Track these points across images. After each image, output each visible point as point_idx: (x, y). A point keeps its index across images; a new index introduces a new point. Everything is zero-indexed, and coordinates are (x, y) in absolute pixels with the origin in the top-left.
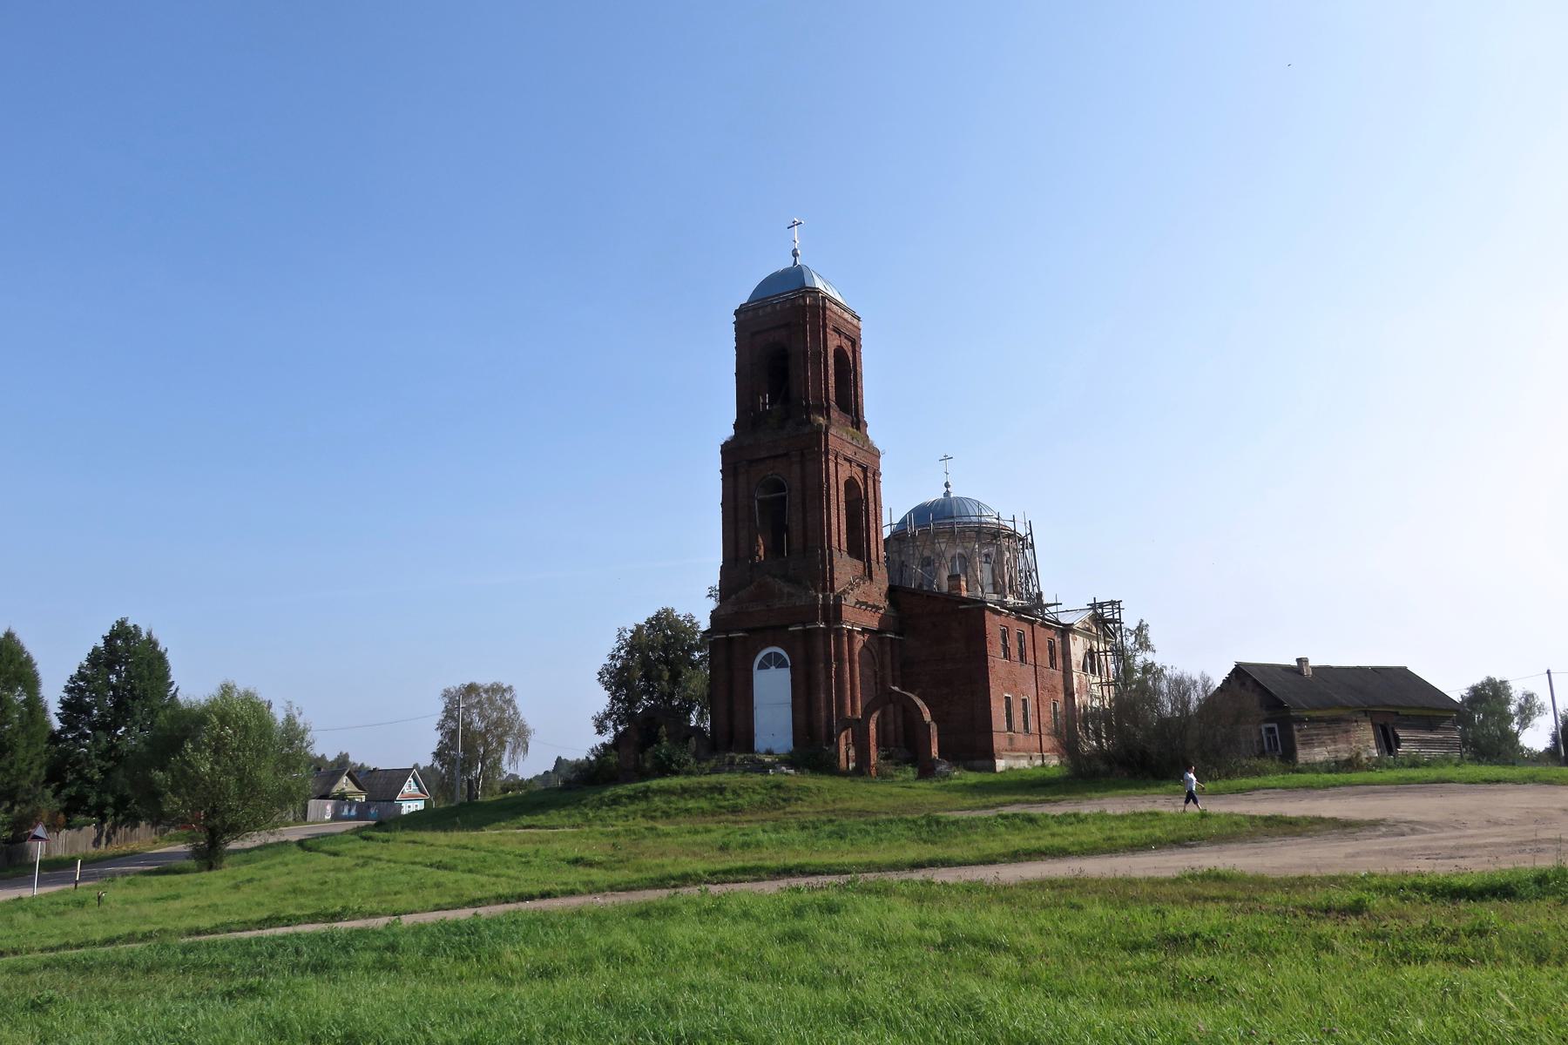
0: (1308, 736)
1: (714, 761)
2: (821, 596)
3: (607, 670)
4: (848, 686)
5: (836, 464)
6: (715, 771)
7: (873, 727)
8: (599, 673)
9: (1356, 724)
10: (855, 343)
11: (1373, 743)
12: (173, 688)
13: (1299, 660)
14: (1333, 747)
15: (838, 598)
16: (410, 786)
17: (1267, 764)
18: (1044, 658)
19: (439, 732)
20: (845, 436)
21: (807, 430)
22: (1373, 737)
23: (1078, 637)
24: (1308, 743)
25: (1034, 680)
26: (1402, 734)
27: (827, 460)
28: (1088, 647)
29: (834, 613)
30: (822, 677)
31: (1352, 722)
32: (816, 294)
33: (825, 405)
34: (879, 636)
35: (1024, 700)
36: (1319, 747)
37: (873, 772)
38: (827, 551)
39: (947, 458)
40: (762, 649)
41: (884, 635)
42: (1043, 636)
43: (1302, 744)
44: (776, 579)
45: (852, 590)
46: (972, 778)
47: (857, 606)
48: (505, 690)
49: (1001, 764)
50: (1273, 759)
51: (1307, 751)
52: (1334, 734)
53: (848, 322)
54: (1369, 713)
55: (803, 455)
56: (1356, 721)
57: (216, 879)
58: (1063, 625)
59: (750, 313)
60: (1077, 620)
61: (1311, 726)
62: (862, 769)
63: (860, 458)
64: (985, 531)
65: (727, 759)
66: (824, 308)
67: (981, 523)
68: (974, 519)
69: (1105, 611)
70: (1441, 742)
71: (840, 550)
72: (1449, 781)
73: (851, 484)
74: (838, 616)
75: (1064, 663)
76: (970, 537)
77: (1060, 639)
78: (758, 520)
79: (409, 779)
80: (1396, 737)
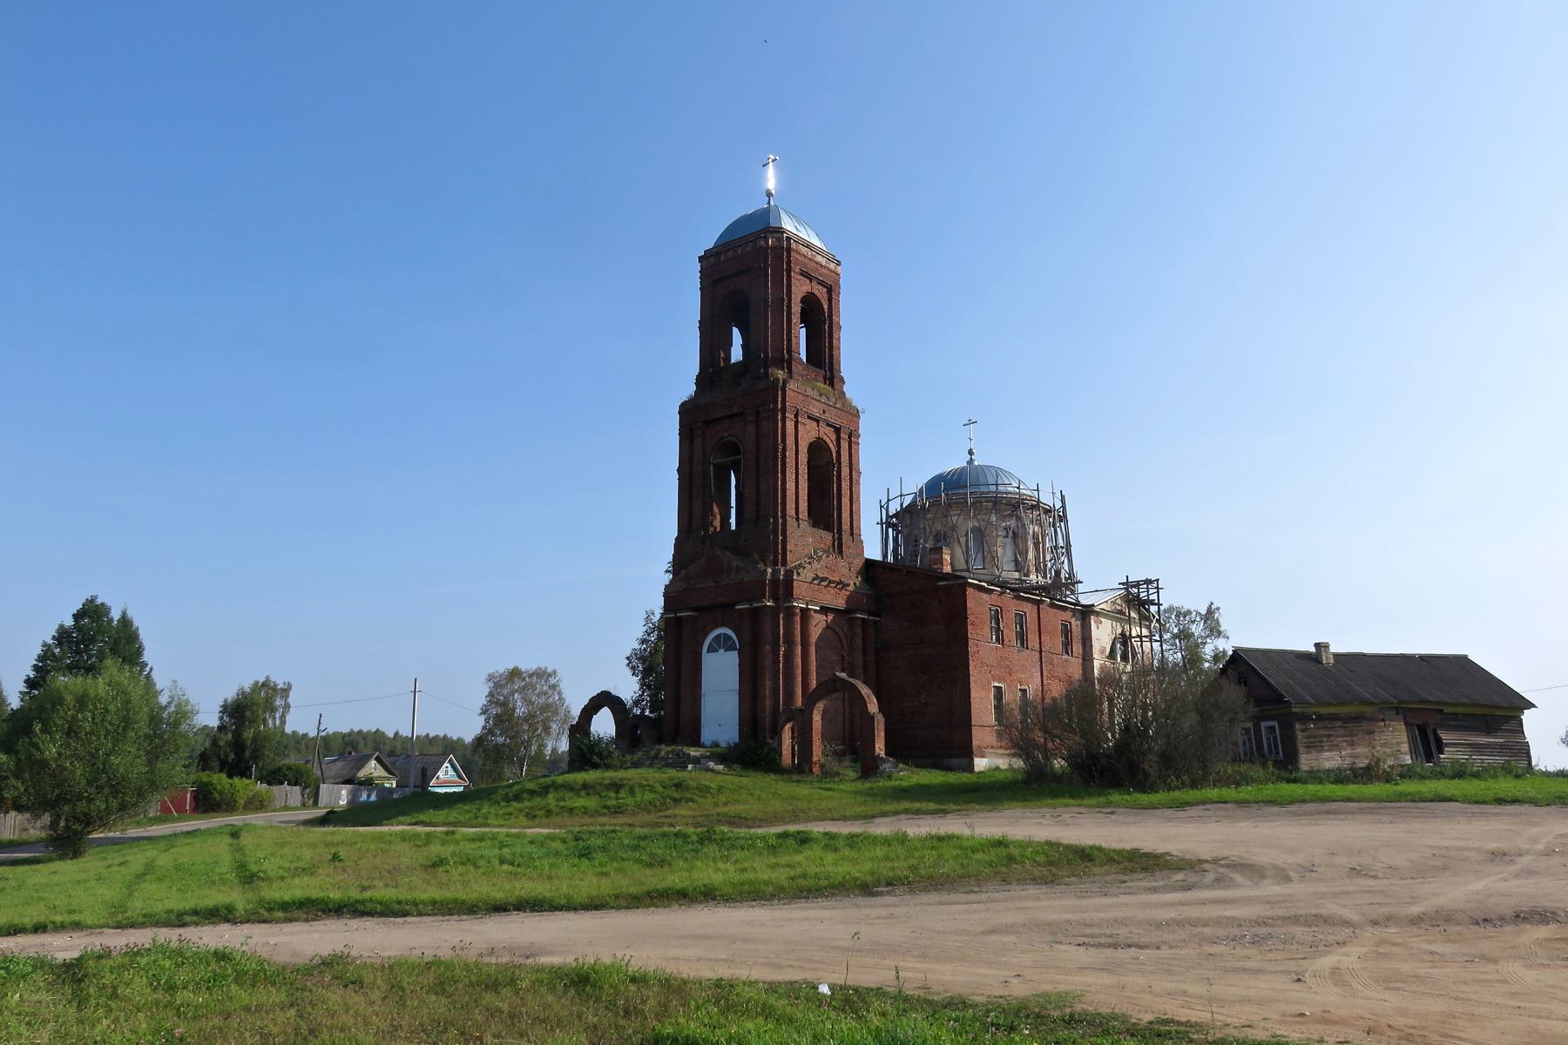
0: (1315, 737)
1: (641, 753)
2: (769, 570)
3: (636, 654)
4: (799, 672)
5: (796, 423)
6: (636, 765)
7: (817, 718)
8: (628, 658)
9: (1382, 724)
10: (831, 290)
11: (1405, 747)
12: (148, 669)
13: (1317, 645)
14: (1349, 751)
15: (789, 573)
16: (447, 773)
17: (1257, 771)
18: (1054, 642)
19: (483, 717)
20: (810, 392)
21: (763, 384)
22: (1406, 739)
23: (1103, 620)
24: (1315, 745)
25: (1039, 666)
26: (1446, 737)
27: (784, 419)
28: (1119, 631)
29: (784, 589)
30: (768, 663)
31: (1378, 721)
32: (780, 235)
33: (786, 355)
34: (849, 616)
35: (998, 689)
36: (1330, 750)
37: (816, 769)
38: (780, 521)
39: (971, 422)
40: (712, 629)
41: (854, 615)
42: (1053, 618)
43: (1307, 747)
44: (727, 552)
45: (810, 563)
46: (952, 778)
47: (816, 582)
48: (549, 675)
49: (980, 764)
50: (1264, 765)
51: (1314, 755)
52: (1351, 736)
53: (822, 266)
54: (1401, 710)
55: (758, 413)
56: (1383, 720)
57: (66, 869)
58: (1083, 606)
59: (711, 259)
60: (1099, 601)
61: (1320, 725)
62: (803, 766)
63: (831, 416)
64: (1004, 501)
65: (653, 753)
66: (789, 250)
67: (997, 493)
68: (993, 488)
69: (1141, 590)
70: (1501, 746)
71: (797, 519)
72: (1450, 800)
73: (817, 448)
74: (789, 594)
75: (1084, 648)
76: (987, 509)
77: (1079, 623)
78: (713, 488)
79: (445, 765)
80: (1439, 742)
